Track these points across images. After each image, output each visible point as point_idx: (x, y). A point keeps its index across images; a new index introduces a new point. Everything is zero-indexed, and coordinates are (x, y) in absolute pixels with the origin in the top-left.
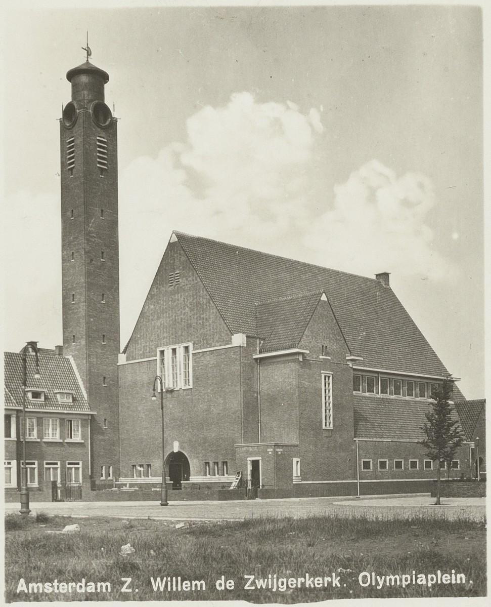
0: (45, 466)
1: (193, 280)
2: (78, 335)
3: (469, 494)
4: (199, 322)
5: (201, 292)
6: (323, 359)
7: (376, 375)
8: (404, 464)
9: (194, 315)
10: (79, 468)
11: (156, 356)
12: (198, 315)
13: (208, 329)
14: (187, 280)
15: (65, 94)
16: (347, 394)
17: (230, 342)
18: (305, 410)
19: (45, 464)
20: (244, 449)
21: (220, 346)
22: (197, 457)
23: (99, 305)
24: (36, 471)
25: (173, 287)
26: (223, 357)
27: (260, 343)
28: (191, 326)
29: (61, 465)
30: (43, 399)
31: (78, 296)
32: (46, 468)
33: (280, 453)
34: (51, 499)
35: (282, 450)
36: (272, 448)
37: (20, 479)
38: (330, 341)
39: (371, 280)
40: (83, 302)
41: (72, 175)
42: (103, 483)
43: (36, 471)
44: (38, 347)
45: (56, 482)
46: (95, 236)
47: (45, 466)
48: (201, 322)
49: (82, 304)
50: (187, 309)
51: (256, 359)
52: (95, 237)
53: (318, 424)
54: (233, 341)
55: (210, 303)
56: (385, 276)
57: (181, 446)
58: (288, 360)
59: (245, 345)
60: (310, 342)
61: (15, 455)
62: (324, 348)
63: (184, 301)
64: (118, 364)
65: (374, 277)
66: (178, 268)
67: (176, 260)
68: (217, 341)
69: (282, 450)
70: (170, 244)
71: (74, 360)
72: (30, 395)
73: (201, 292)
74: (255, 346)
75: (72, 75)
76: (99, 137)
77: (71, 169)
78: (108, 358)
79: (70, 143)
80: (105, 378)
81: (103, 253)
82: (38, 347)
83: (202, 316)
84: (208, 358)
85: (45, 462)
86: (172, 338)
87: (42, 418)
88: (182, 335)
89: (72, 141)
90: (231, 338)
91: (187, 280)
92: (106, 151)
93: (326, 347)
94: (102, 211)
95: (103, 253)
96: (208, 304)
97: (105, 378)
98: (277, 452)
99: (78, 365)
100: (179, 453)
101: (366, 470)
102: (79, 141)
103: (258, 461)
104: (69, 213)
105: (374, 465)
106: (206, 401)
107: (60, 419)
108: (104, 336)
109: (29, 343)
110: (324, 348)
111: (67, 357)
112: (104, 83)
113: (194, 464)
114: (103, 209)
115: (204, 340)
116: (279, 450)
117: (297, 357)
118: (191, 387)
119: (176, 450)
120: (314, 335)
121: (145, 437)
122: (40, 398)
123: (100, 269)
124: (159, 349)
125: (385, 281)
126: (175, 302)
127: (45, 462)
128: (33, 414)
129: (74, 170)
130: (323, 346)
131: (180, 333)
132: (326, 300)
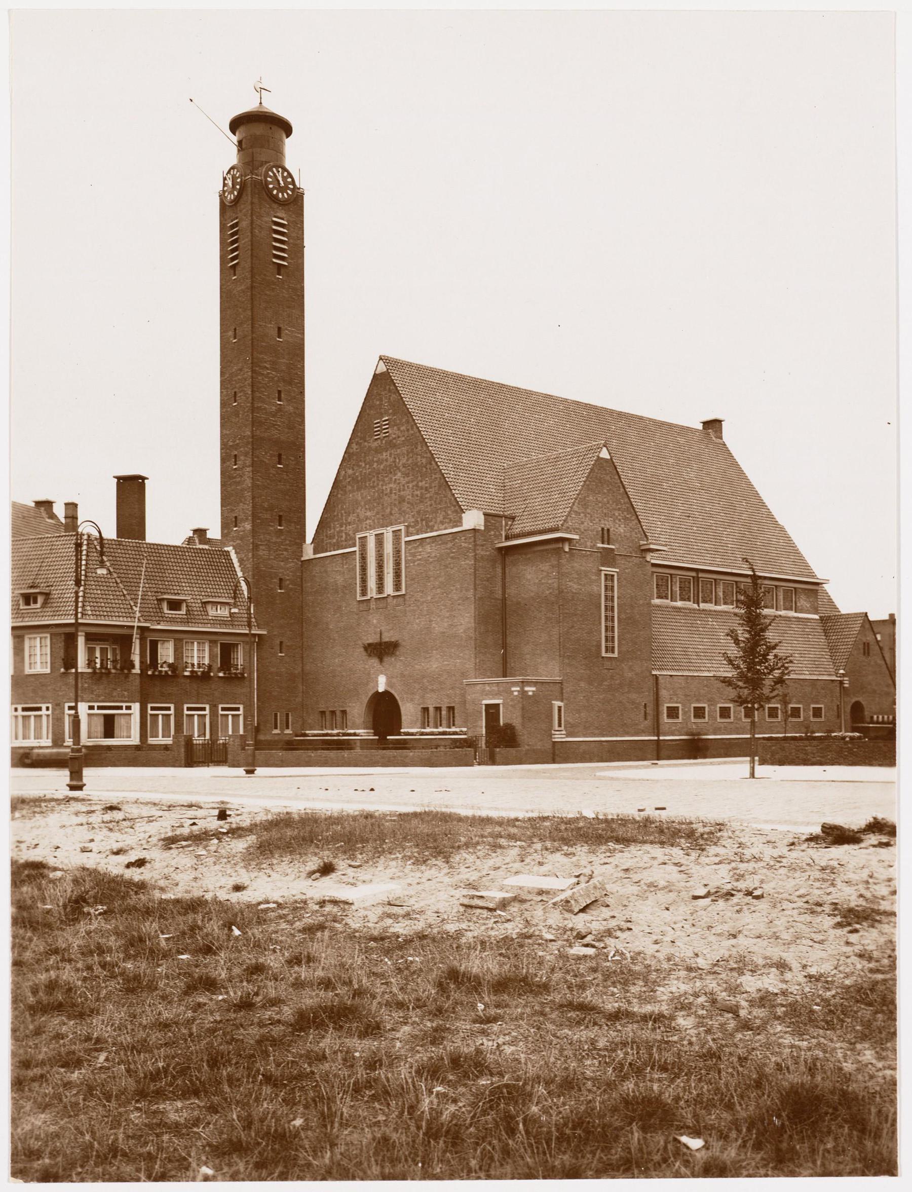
0: (221, 712)
1: (408, 430)
2: (242, 516)
3: (814, 760)
4: (416, 493)
5: (419, 448)
6: (604, 548)
7: (694, 574)
8: (734, 712)
9: (408, 483)
10: (238, 715)
11: (354, 546)
12: (414, 483)
13: (429, 503)
14: (399, 429)
15: (226, 153)
16: (641, 602)
17: (459, 522)
18: (573, 627)
19: (66, 708)
20: (478, 687)
21: (445, 529)
22: (412, 700)
23: (273, 471)
24: (172, 718)
25: (379, 441)
26: (450, 545)
27: (506, 525)
28: (404, 501)
29: (210, 709)
30: (183, 611)
31: (242, 458)
32: (151, 715)
33: (530, 693)
34: (183, 762)
35: (534, 689)
36: (518, 686)
37: (41, 728)
38: (614, 521)
39: (697, 431)
40: (249, 466)
41: (235, 275)
42: (276, 738)
43: (172, 718)
44: (208, 536)
45: (192, 736)
46: (268, 366)
47: (221, 712)
48: (418, 493)
49: (248, 469)
50: (399, 474)
51: (500, 549)
52: (267, 369)
53: (593, 649)
54: (464, 521)
55: (431, 464)
56: (713, 425)
57: (389, 683)
58: (546, 550)
59: (483, 528)
60: (582, 523)
61: (138, 696)
62: (605, 532)
63: (394, 462)
64: (303, 559)
65: (700, 427)
66: (386, 413)
67: (385, 400)
68: (442, 523)
69: (534, 689)
70: (375, 376)
71: (236, 553)
72: (165, 606)
73: (419, 448)
74: (498, 529)
75: (236, 124)
76: (275, 217)
77: (234, 266)
78: (286, 550)
79: (233, 227)
80: (281, 580)
81: (279, 392)
82: (208, 536)
83: (420, 484)
84: (428, 548)
85: (186, 706)
86: (379, 519)
87: (181, 640)
88: (391, 514)
89: (236, 225)
90: (461, 518)
91: (399, 429)
92: (286, 239)
93: (608, 530)
94: (279, 329)
95: (279, 392)
96: (428, 466)
97: (281, 580)
98: (527, 692)
99: (241, 561)
100: (386, 693)
101: (671, 721)
102: (245, 224)
103: (497, 706)
104: (231, 333)
105: (685, 713)
106: (425, 613)
107: (211, 642)
108: (280, 517)
109: (196, 531)
110: (605, 532)
111: (226, 549)
112: (284, 136)
113: (409, 711)
114: (281, 326)
115: (422, 520)
116: (530, 690)
117: (561, 546)
118: (403, 592)
119: (381, 689)
120: (589, 511)
121: (339, 669)
122: (180, 610)
123: (273, 416)
124: (358, 536)
125: (716, 432)
126: (382, 463)
127: (186, 706)
128: (205, 637)
129: (238, 269)
130: (603, 529)
131: (388, 510)
132: (609, 457)
